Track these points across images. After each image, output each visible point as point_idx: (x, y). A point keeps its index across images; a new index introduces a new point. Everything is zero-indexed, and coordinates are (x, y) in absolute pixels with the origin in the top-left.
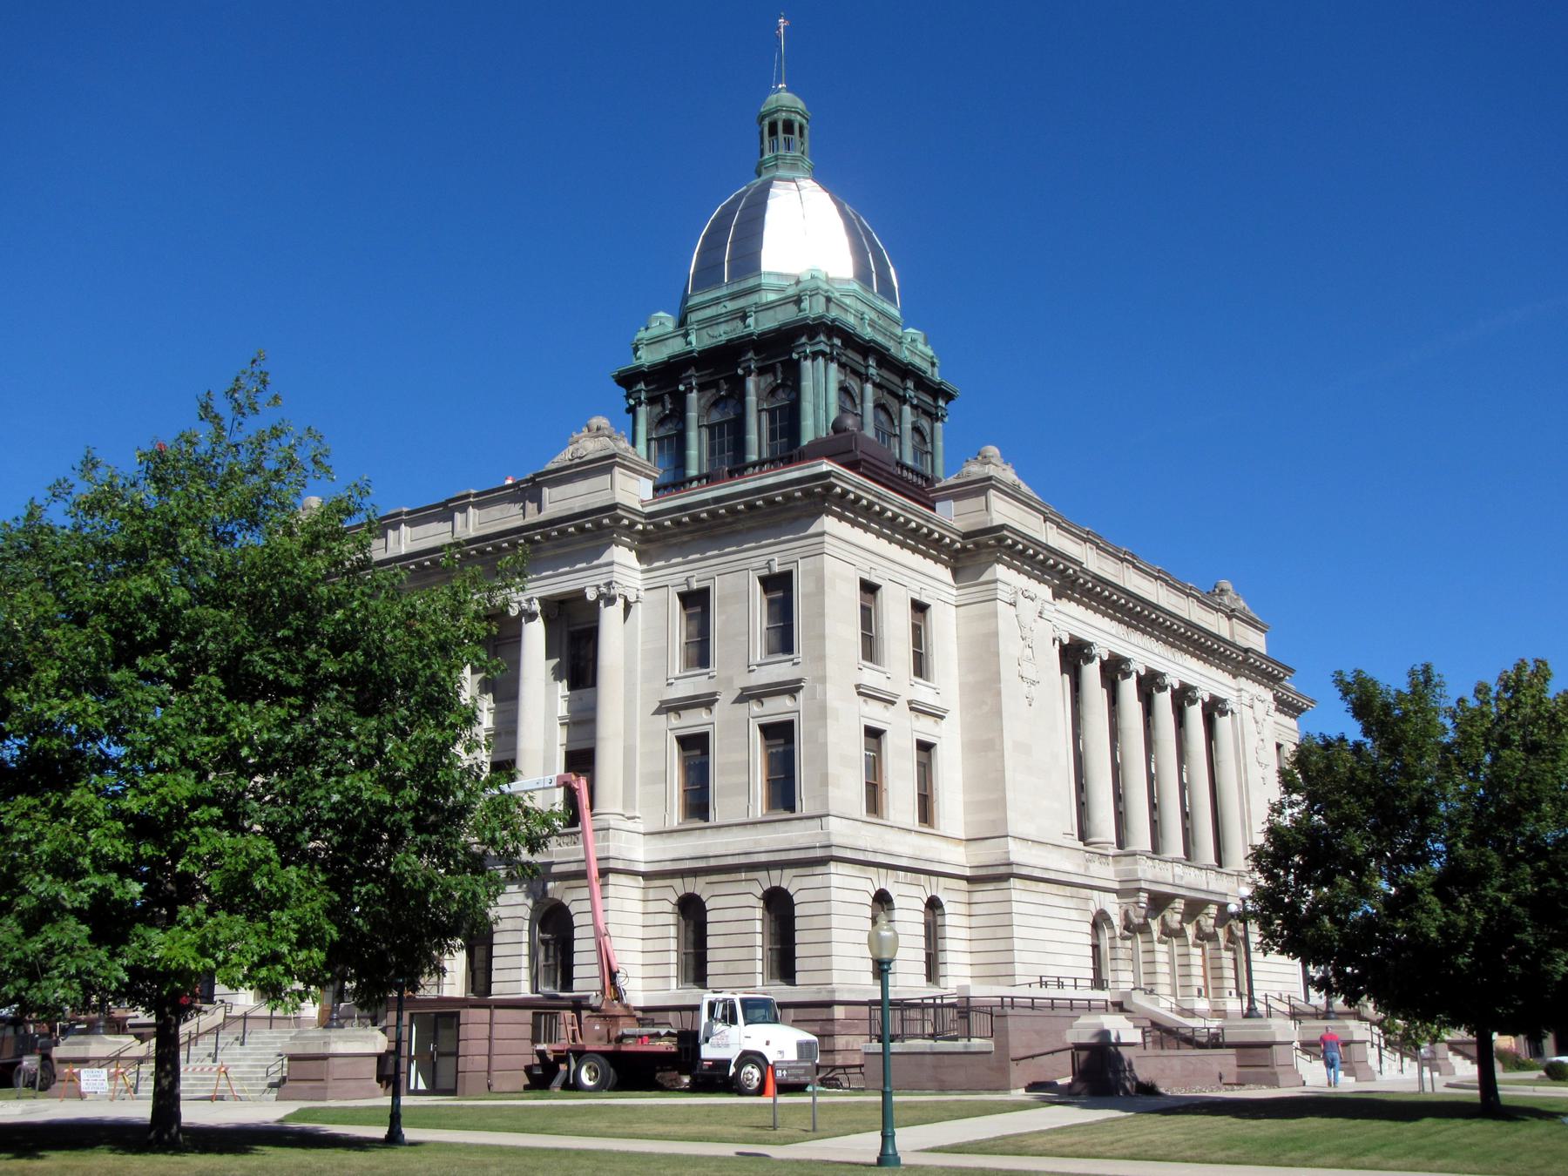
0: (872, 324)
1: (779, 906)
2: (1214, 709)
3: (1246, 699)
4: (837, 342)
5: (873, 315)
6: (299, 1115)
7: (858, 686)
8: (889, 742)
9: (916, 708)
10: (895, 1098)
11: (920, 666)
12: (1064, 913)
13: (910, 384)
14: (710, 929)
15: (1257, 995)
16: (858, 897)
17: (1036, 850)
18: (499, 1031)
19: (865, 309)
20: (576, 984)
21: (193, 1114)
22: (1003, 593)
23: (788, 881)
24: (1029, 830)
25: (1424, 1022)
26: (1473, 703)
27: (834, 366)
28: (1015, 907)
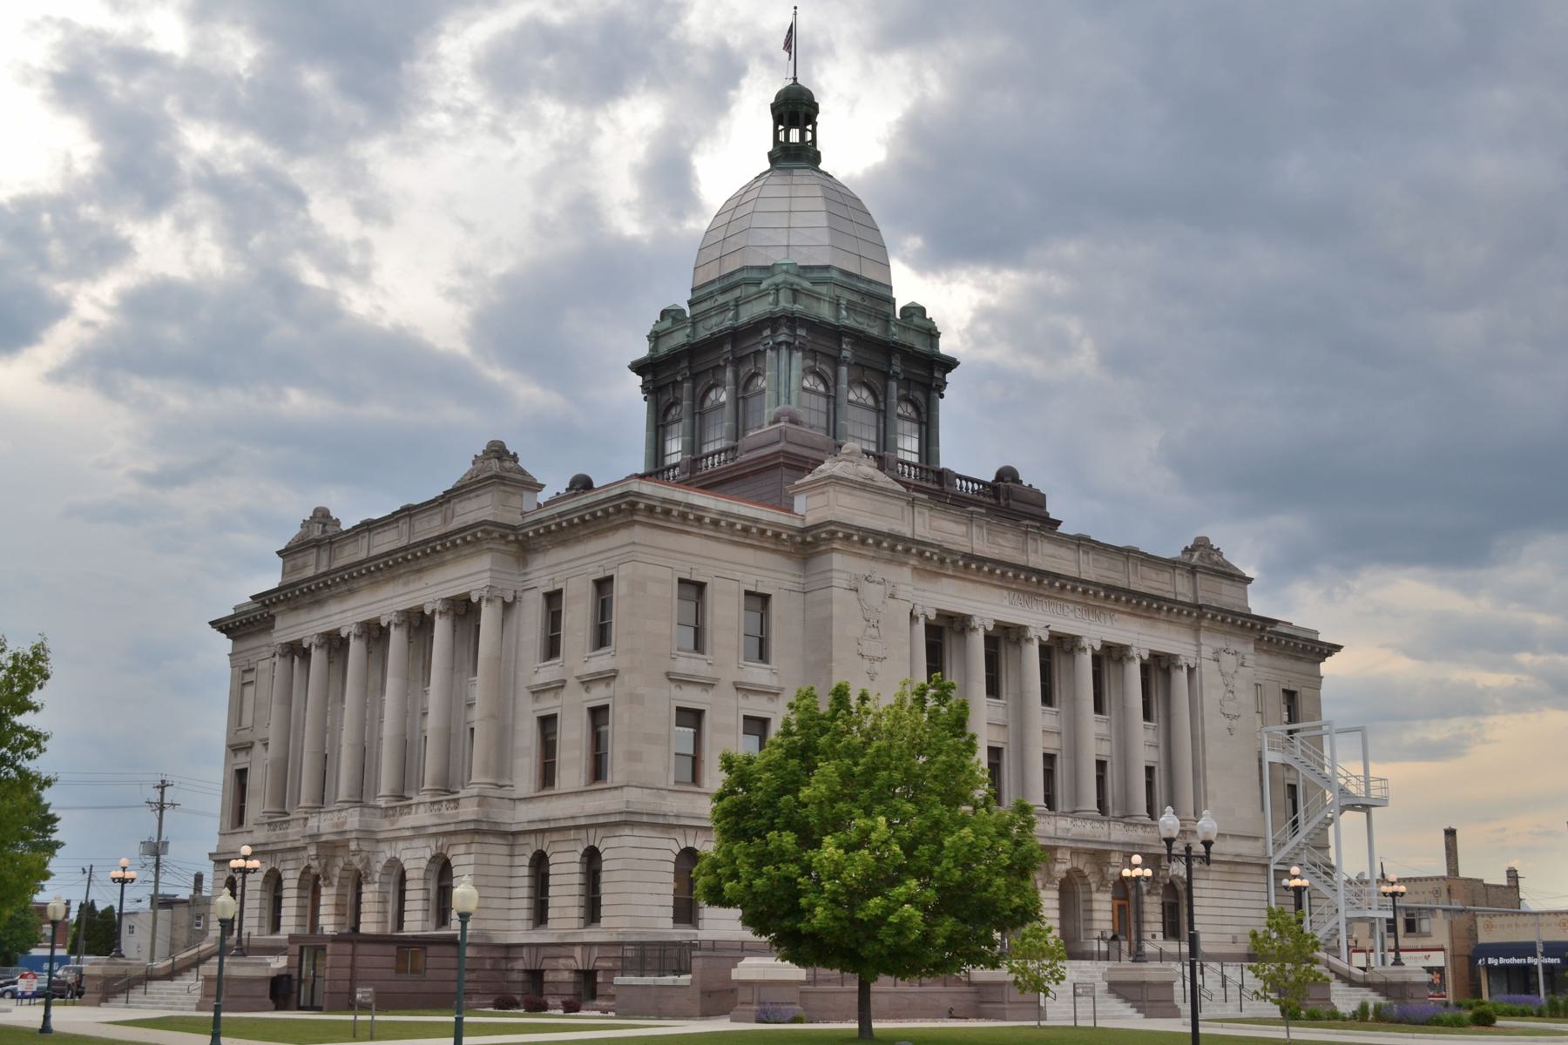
0: (851, 307)
1: (592, 858)
3: (1207, 651)
4: (801, 332)
5: (855, 298)
7: (668, 674)
10: (856, 1026)
14: (552, 880)
15: (245, 931)
16: (658, 855)
18: (360, 960)
19: (838, 291)
22: (840, 580)
23: (544, 844)
26: (824, 708)
27: (798, 355)
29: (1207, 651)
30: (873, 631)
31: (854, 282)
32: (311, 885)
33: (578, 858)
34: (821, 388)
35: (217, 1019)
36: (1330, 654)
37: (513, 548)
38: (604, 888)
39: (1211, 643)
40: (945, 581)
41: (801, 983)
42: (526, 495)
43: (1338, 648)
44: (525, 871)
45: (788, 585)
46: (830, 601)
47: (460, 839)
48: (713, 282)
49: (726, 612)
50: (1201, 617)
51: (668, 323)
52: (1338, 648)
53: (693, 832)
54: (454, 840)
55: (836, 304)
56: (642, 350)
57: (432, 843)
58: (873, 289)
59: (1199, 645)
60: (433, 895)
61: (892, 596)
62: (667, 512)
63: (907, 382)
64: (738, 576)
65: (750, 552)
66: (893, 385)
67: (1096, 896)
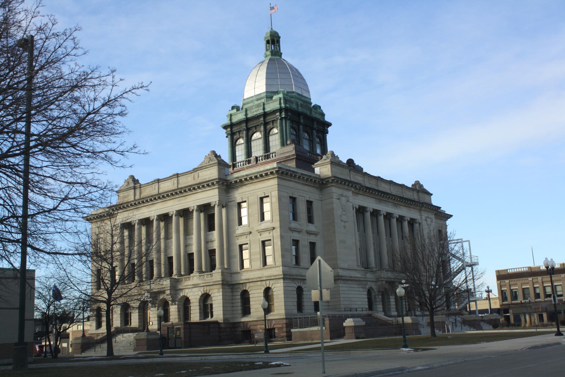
2: (412, 222)
3: (424, 218)
5: (302, 103)
6: (139, 353)
8: (301, 244)
9: (309, 233)
11: (310, 220)
12: (358, 289)
13: (315, 124)
16: (291, 289)
17: (347, 272)
19: (297, 100)
20: (214, 317)
21: (116, 353)
22: (335, 196)
24: (345, 266)
25: (286, 323)
28: (341, 289)
29: (424, 218)
30: (344, 213)
31: (301, 97)
32: (143, 308)
33: (263, 291)
34: (294, 133)
35: (266, 346)
36: (450, 218)
37: (224, 187)
38: (296, 300)
39: (425, 215)
40: (360, 196)
41: (364, 326)
42: (226, 169)
43: (451, 216)
44: (239, 297)
45: (317, 198)
46: (333, 203)
47: (214, 287)
48: (252, 97)
49: (302, 208)
50: (423, 206)
51: (235, 111)
52: (451, 216)
53: (299, 281)
54: (211, 287)
55: (297, 105)
56: (227, 121)
57: (202, 289)
58: (306, 99)
59: (421, 215)
60: (202, 307)
61: (348, 201)
62: (287, 174)
63: (318, 131)
64: (304, 195)
65: (172, 201)
66: (315, 132)
67: (391, 297)
